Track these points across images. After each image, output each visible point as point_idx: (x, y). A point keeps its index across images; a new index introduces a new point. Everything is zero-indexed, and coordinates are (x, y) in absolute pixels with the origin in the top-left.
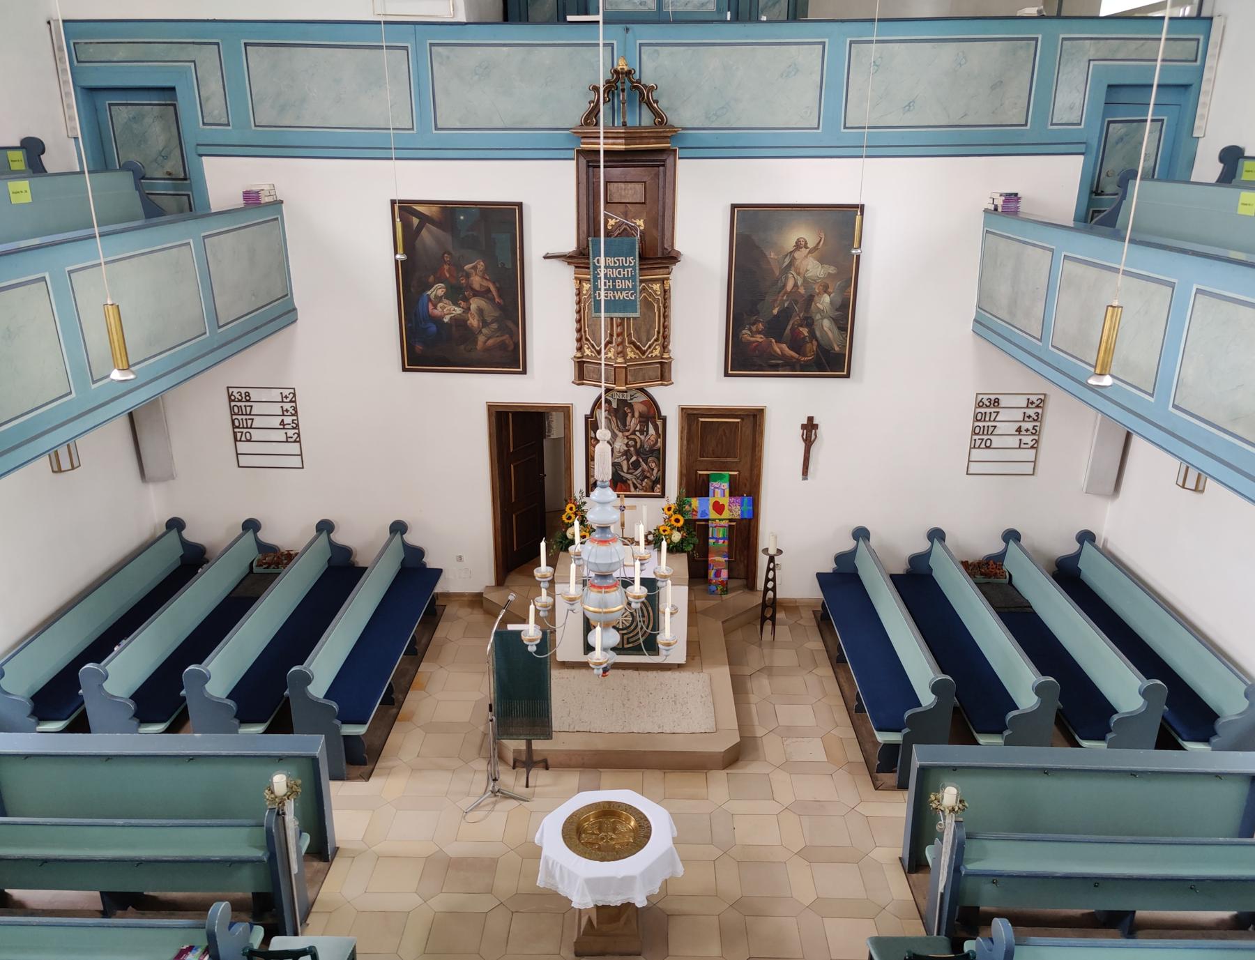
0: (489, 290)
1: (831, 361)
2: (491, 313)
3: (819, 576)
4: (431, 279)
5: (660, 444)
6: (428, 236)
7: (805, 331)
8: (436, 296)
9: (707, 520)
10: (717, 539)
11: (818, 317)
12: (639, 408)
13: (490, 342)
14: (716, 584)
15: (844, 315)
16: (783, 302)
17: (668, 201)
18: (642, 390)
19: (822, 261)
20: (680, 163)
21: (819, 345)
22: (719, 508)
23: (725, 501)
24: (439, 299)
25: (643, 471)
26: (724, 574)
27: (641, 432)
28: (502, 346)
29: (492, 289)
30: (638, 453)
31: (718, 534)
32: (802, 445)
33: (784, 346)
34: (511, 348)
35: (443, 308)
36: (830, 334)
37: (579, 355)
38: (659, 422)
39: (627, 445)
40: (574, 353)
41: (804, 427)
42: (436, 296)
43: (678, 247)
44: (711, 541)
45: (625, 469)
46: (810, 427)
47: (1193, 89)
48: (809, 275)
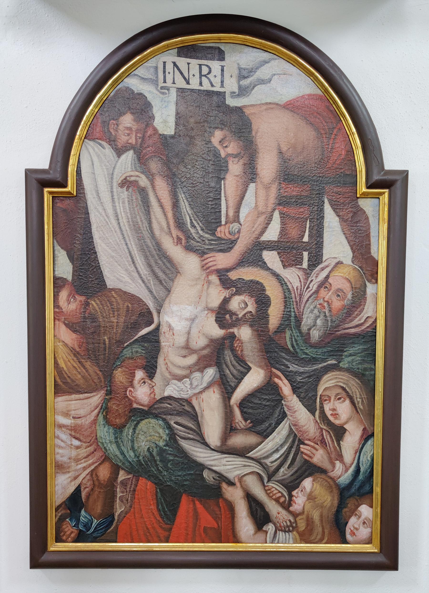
5: (249, 539)
12: (275, 135)
25: (296, 439)
27: (289, 250)
30: (272, 350)
38: (375, 209)
39: (222, 314)
45: (213, 430)
47: (398, 185)
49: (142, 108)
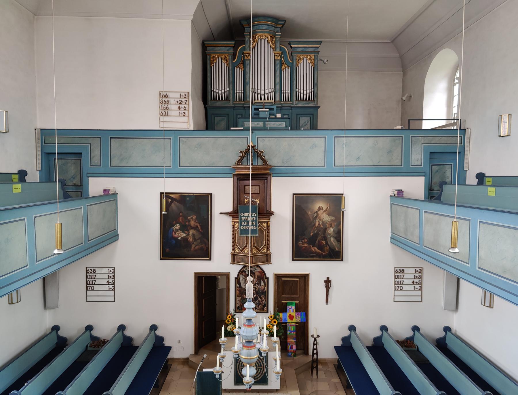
0: (197, 227)
1: (335, 254)
2: (198, 235)
3: (335, 347)
4: (174, 222)
7: (324, 242)
9: (286, 323)
10: (291, 332)
11: (329, 236)
13: (197, 247)
14: (291, 352)
15: (339, 235)
16: (315, 231)
17: (268, 193)
18: (258, 266)
19: (329, 215)
20: (273, 178)
21: (330, 248)
22: (291, 317)
23: (294, 314)
24: (177, 230)
26: (294, 347)
27: (258, 284)
28: (202, 249)
29: (199, 226)
31: (291, 329)
32: (325, 290)
33: (316, 248)
34: (205, 249)
35: (178, 234)
36: (334, 243)
37: (233, 252)
38: (266, 280)
40: (231, 251)
41: (325, 282)
43: (272, 210)
44: (288, 332)
46: (328, 282)
48: (324, 220)
49: (245, 272)
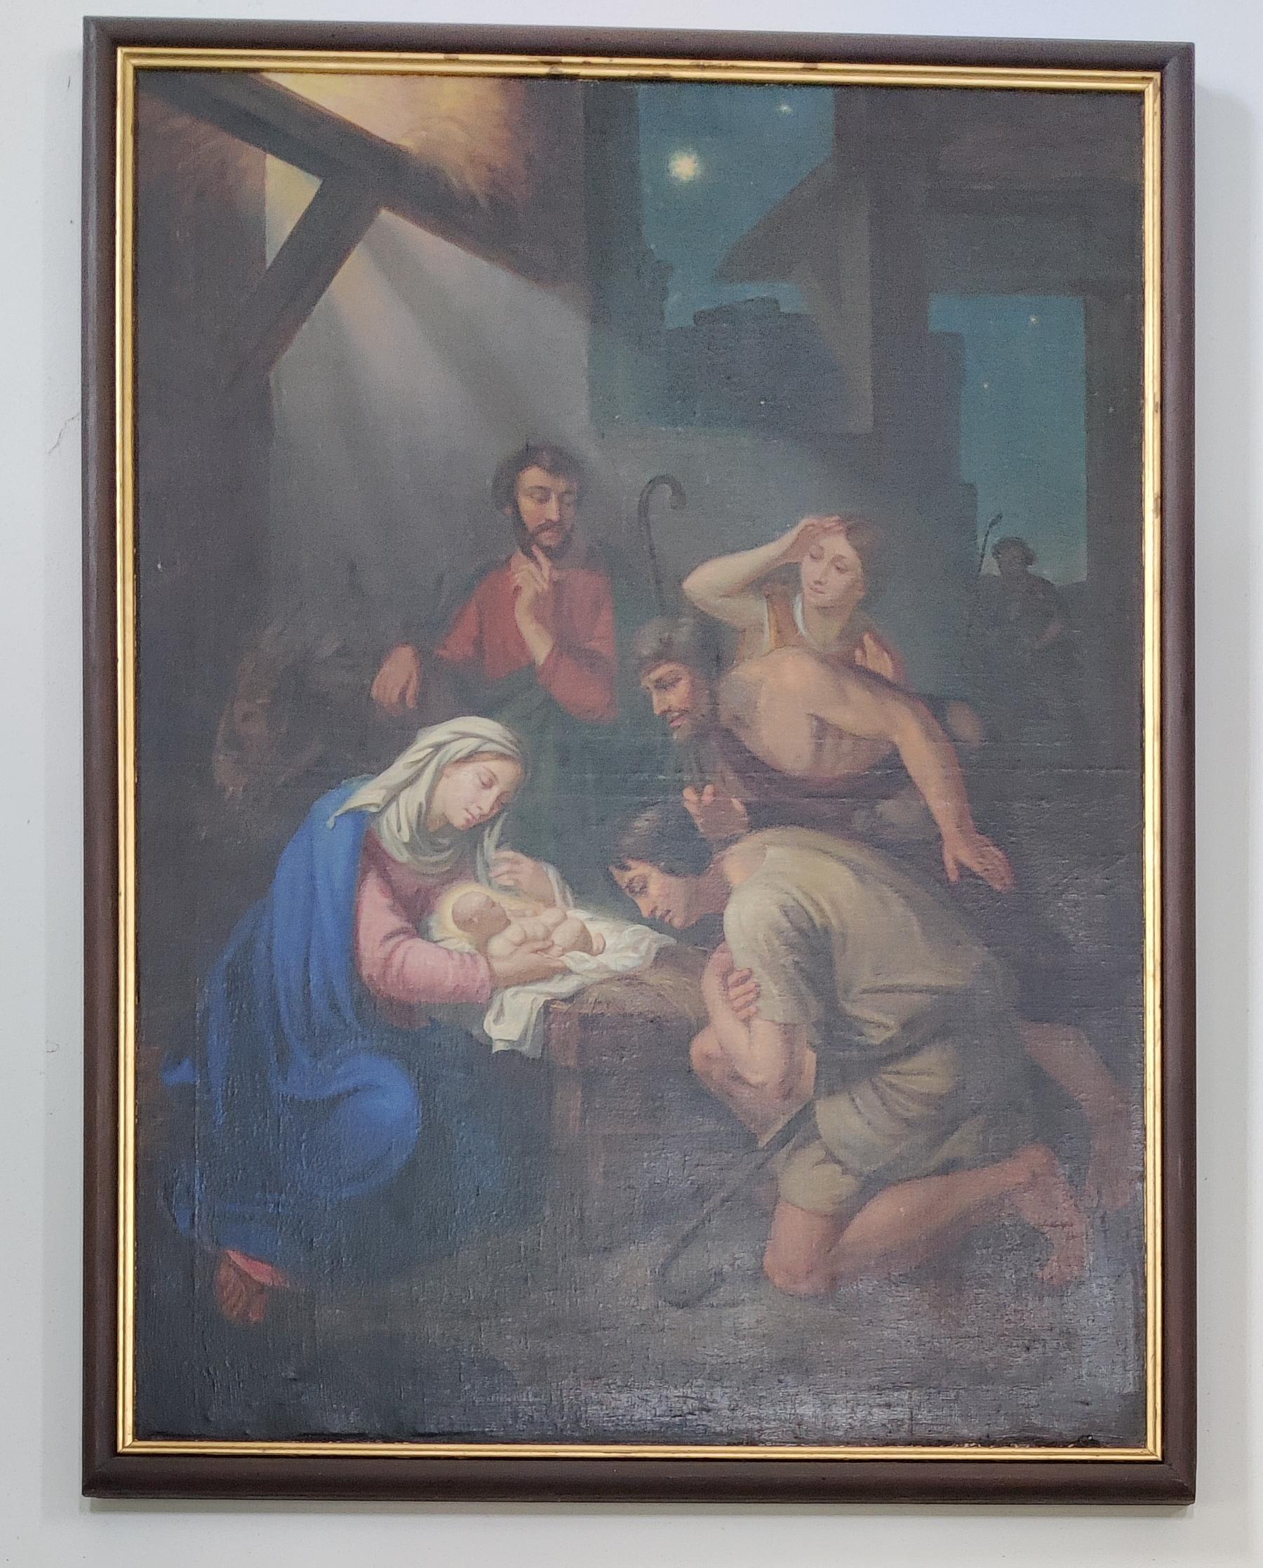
4: (397, 674)
6: (399, 329)
8: (429, 830)
24: (457, 848)
35: (483, 927)
42: (429, 830)
